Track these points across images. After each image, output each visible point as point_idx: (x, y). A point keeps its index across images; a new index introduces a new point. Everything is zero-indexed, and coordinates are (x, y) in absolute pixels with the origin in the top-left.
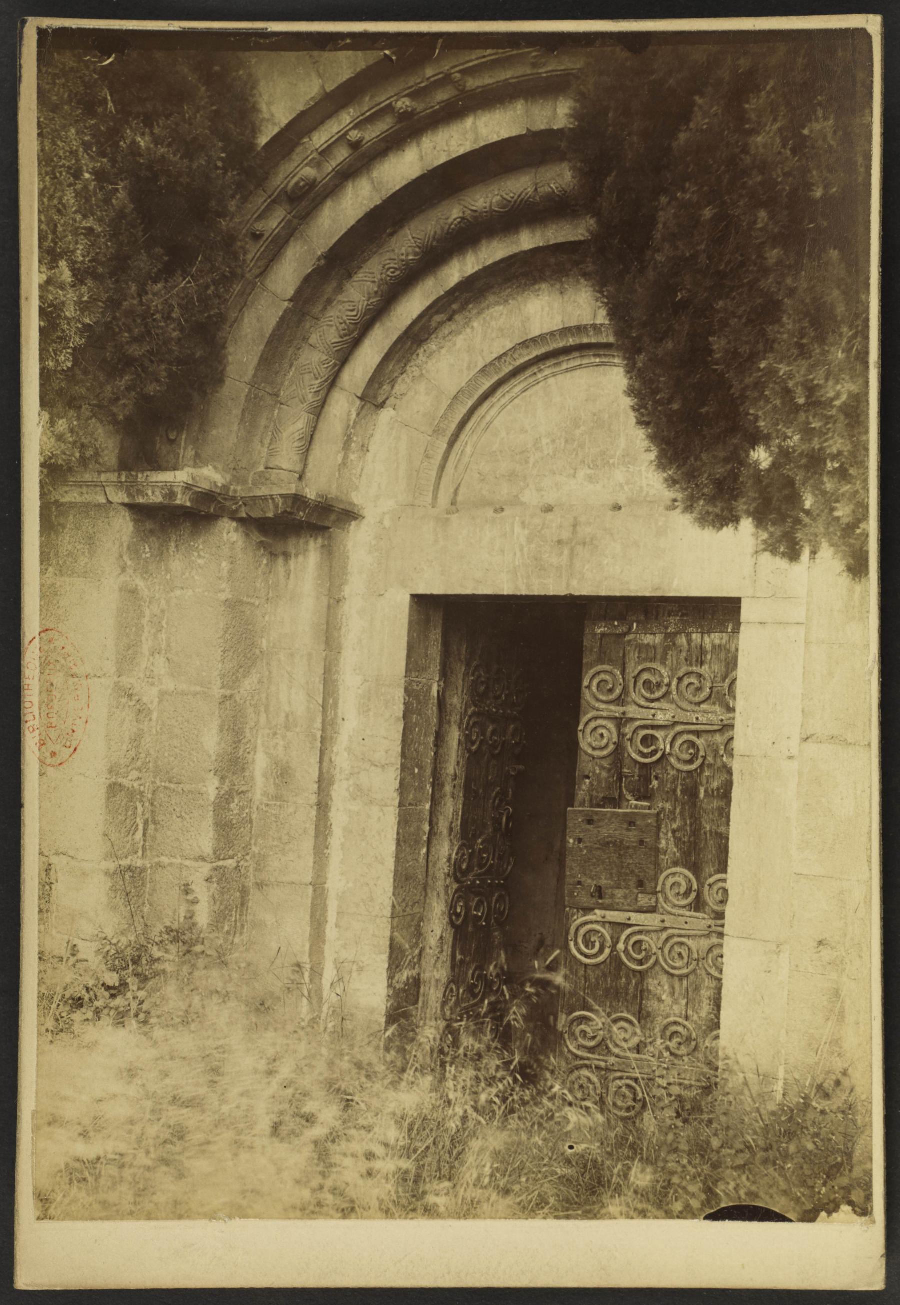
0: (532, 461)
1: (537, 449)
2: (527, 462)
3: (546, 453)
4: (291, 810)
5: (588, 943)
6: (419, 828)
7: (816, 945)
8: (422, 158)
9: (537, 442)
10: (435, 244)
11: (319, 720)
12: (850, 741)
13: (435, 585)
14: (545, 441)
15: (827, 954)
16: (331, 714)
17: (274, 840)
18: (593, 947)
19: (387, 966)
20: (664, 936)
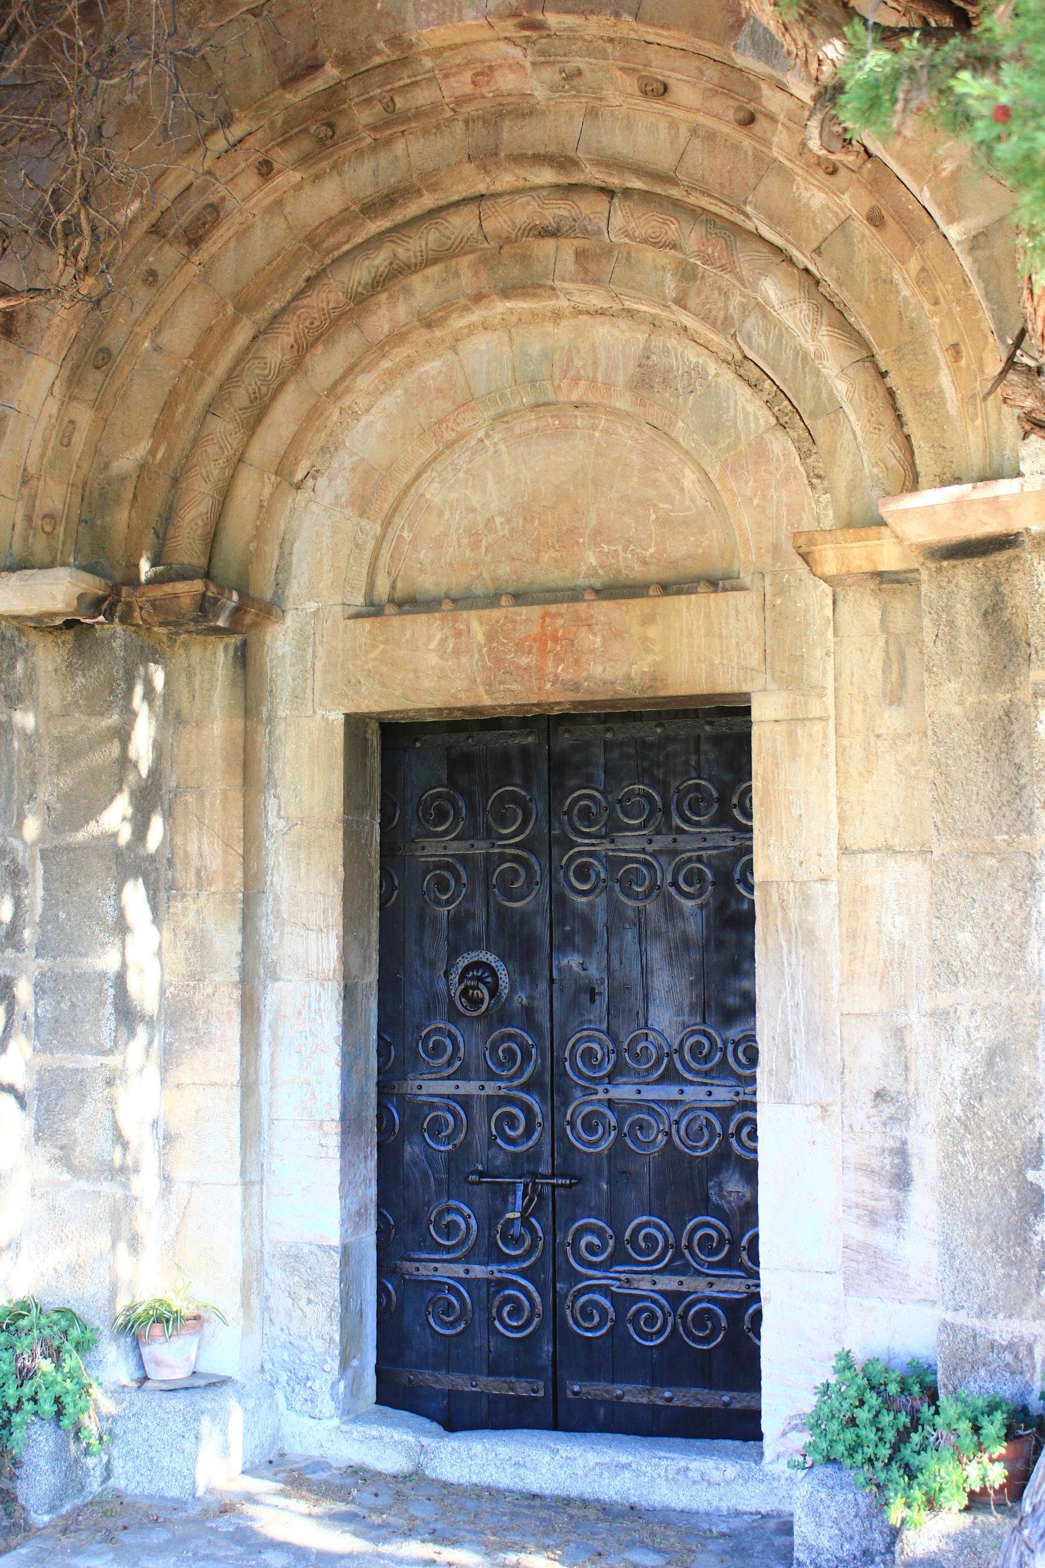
0: (484, 544)
1: (490, 531)
2: (478, 547)
3: (500, 534)
4: (209, 990)
5: (590, 1129)
6: (220, 1548)
7: (872, 1097)
8: (344, 191)
9: (490, 521)
10: (360, 290)
11: (239, 874)
12: (897, 848)
13: (374, 701)
14: (499, 520)
15: (887, 1110)
16: (254, 865)
17: (187, 1030)
18: (593, 1319)
19: (338, 1181)
20: (681, 1109)
